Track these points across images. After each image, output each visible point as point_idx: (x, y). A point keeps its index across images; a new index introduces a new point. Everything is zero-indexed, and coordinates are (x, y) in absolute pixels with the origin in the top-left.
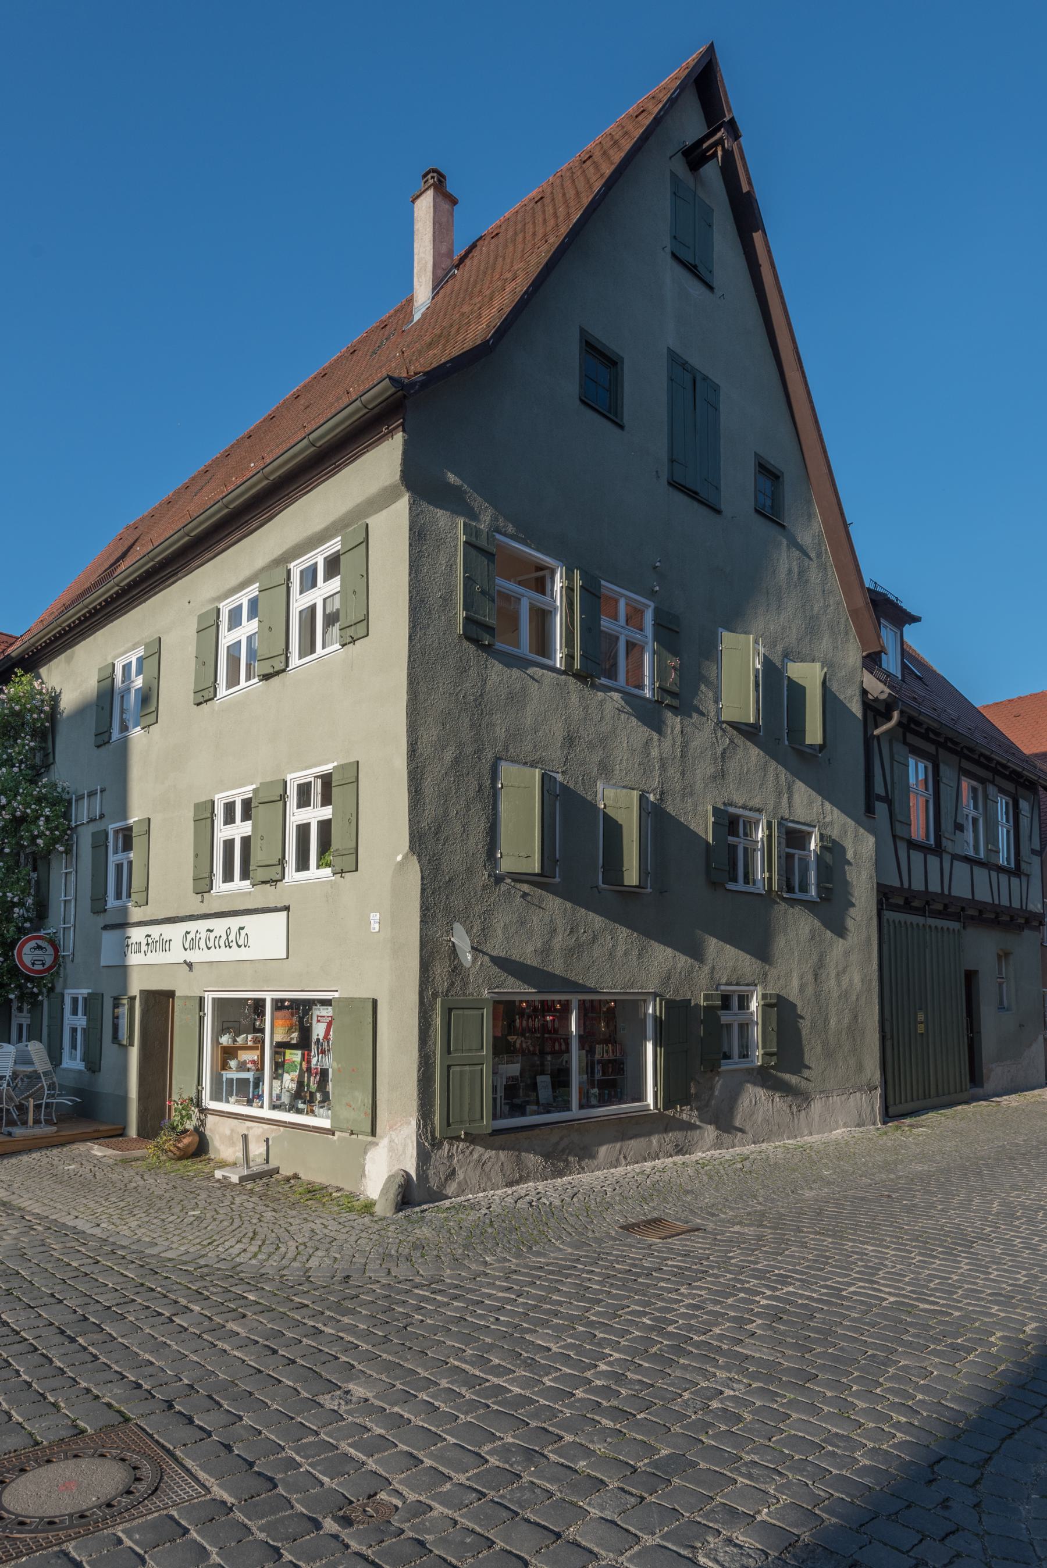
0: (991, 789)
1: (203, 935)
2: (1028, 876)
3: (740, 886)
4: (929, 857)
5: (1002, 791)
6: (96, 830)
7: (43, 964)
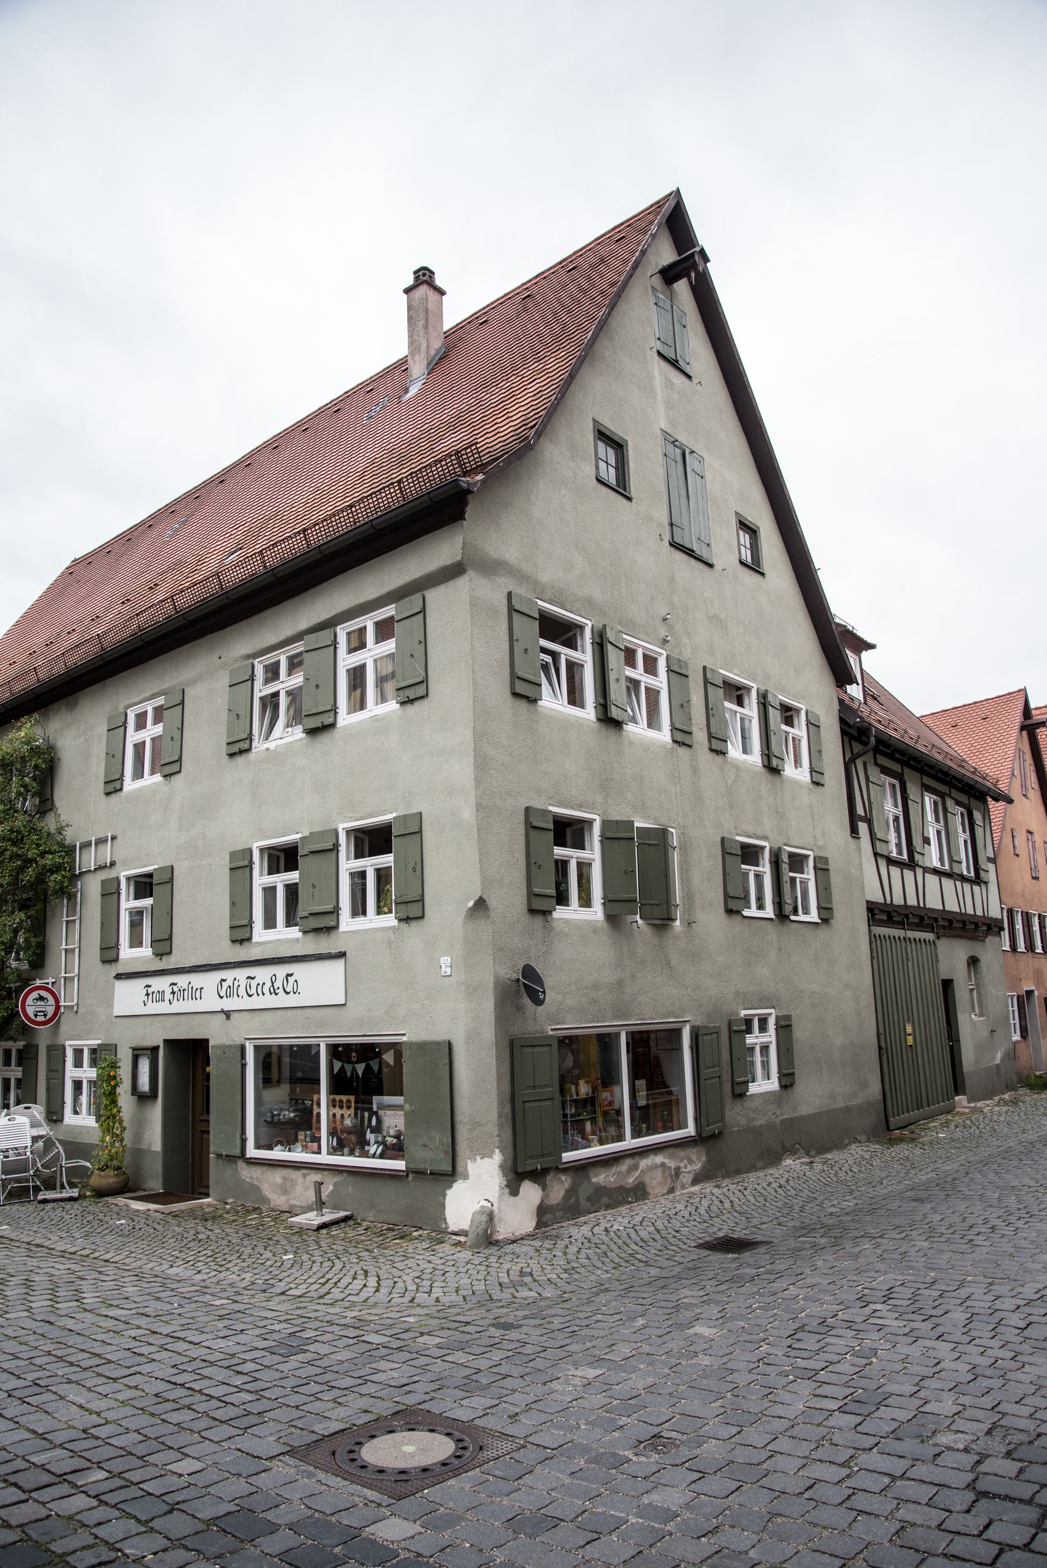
0: (950, 803)
1: (243, 982)
2: (986, 883)
3: (753, 912)
4: (905, 871)
5: (958, 803)
6: (103, 878)
7: (45, 1015)
